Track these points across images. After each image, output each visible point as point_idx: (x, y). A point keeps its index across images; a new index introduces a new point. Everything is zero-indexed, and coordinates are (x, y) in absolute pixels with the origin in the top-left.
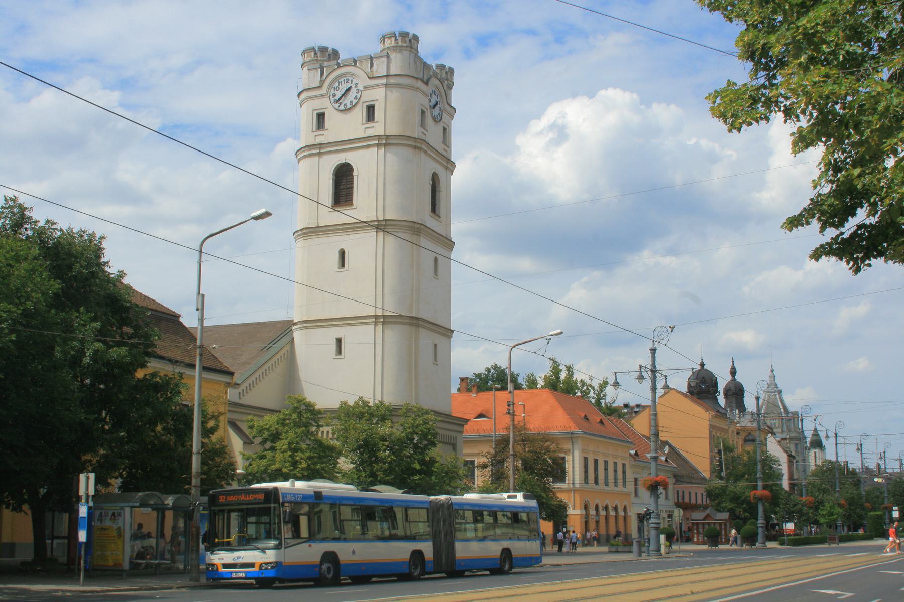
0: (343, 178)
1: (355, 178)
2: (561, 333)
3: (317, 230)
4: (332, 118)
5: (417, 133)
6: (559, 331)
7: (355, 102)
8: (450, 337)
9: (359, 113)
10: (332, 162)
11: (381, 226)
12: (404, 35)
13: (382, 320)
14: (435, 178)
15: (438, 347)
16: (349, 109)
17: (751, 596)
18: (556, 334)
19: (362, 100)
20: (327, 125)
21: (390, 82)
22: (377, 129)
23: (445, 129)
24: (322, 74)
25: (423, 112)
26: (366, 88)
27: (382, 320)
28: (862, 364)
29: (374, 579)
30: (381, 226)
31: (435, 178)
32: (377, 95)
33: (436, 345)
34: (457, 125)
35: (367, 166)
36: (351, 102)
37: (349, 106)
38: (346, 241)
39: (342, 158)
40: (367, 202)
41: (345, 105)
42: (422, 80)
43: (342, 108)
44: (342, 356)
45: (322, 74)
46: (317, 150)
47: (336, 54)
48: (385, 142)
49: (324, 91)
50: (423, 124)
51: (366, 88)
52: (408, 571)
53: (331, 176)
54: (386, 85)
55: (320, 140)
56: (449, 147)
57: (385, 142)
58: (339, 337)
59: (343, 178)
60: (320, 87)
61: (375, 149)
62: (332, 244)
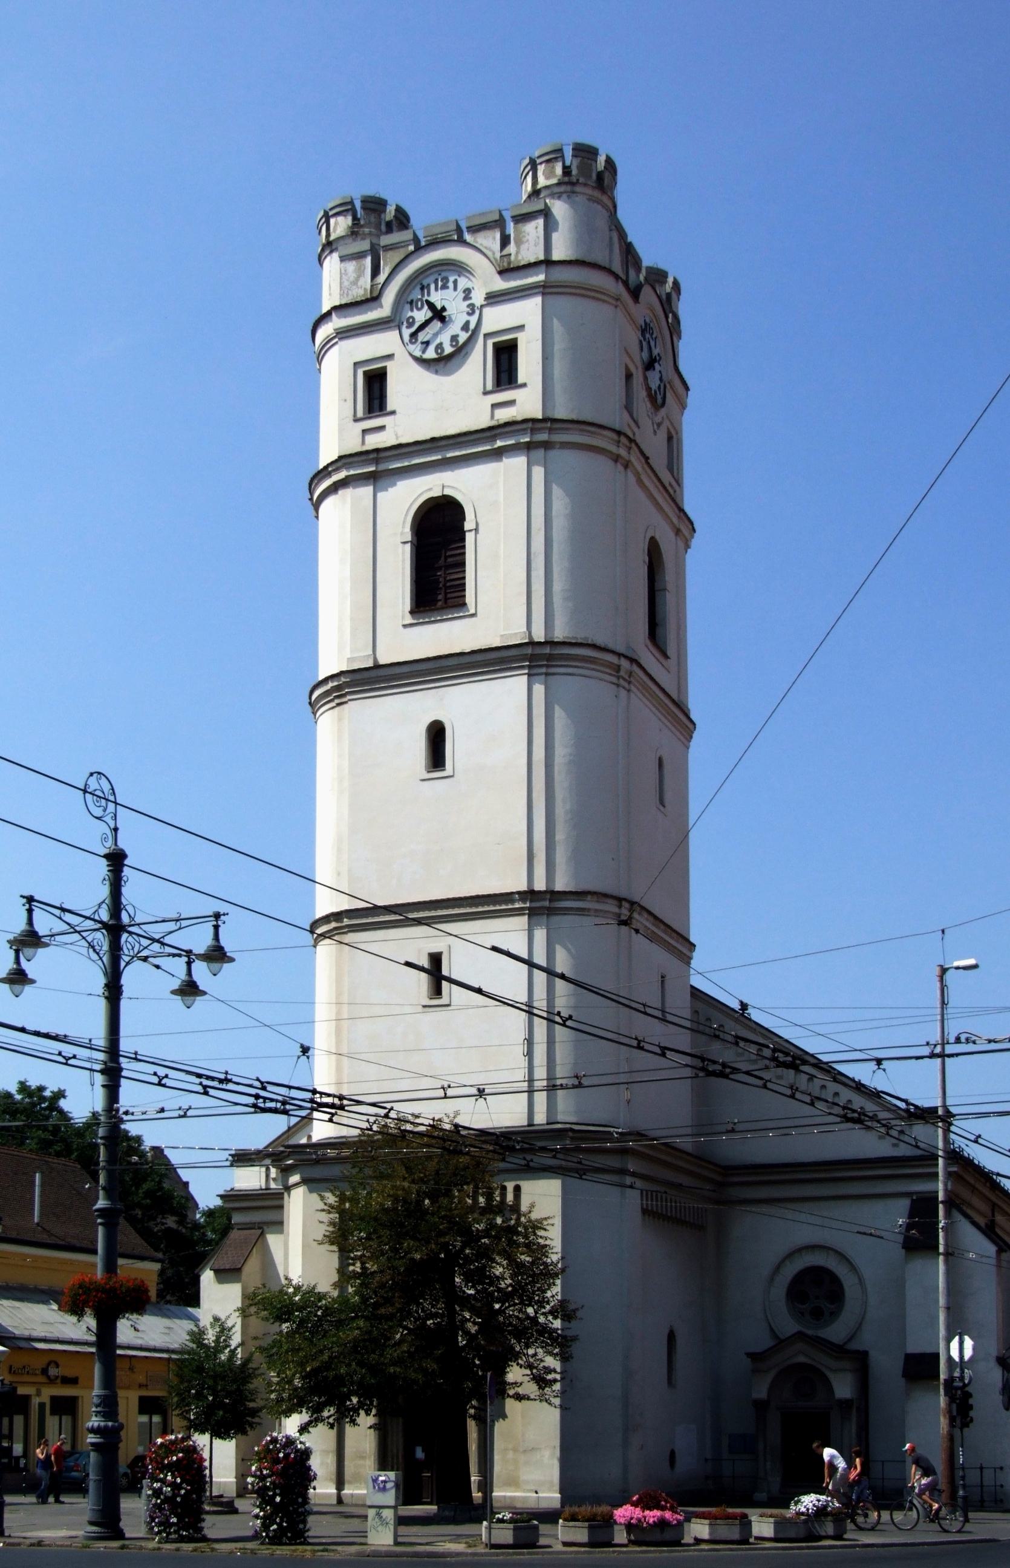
0: (439, 536)
1: (469, 538)
2: (975, 966)
3: (373, 673)
4: (406, 382)
5: (616, 418)
6: (971, 962)
7: (463, 337)
9: (478, 365)
10: (407, 495)
11: (533, 657)
12: (586, 152)
13: (538, 905)
14: (654, 551)
16: (451, 356)
18: (965, 968)
19: (486, 328)
20: (393, 401)
21: (553, 281)
22: (527, 402)
23: (670, 438)
24: (376, 271)
25: (629, 376)
26: (494, 298)
27: (538, 905)
30: (533, 657)
31: (654, 551)
32: (526, 316)
35: (499, 500)
36: (454, 338)
37: (448, 349)
38: (456, 703)
40: (502, 596)
41: (440, 346)
42: (626, 283)
43: (431, 354)
45: (376, 271)
46: (374, 467)
47: (402, 220)
48: (536, 437)
49: (385, 309)
50: (628, 407)
51: (494, 298)
55: (374, 441)
56: (679, 482)
57: (536, 437)
59: (439, 536)
62: (408, 712)
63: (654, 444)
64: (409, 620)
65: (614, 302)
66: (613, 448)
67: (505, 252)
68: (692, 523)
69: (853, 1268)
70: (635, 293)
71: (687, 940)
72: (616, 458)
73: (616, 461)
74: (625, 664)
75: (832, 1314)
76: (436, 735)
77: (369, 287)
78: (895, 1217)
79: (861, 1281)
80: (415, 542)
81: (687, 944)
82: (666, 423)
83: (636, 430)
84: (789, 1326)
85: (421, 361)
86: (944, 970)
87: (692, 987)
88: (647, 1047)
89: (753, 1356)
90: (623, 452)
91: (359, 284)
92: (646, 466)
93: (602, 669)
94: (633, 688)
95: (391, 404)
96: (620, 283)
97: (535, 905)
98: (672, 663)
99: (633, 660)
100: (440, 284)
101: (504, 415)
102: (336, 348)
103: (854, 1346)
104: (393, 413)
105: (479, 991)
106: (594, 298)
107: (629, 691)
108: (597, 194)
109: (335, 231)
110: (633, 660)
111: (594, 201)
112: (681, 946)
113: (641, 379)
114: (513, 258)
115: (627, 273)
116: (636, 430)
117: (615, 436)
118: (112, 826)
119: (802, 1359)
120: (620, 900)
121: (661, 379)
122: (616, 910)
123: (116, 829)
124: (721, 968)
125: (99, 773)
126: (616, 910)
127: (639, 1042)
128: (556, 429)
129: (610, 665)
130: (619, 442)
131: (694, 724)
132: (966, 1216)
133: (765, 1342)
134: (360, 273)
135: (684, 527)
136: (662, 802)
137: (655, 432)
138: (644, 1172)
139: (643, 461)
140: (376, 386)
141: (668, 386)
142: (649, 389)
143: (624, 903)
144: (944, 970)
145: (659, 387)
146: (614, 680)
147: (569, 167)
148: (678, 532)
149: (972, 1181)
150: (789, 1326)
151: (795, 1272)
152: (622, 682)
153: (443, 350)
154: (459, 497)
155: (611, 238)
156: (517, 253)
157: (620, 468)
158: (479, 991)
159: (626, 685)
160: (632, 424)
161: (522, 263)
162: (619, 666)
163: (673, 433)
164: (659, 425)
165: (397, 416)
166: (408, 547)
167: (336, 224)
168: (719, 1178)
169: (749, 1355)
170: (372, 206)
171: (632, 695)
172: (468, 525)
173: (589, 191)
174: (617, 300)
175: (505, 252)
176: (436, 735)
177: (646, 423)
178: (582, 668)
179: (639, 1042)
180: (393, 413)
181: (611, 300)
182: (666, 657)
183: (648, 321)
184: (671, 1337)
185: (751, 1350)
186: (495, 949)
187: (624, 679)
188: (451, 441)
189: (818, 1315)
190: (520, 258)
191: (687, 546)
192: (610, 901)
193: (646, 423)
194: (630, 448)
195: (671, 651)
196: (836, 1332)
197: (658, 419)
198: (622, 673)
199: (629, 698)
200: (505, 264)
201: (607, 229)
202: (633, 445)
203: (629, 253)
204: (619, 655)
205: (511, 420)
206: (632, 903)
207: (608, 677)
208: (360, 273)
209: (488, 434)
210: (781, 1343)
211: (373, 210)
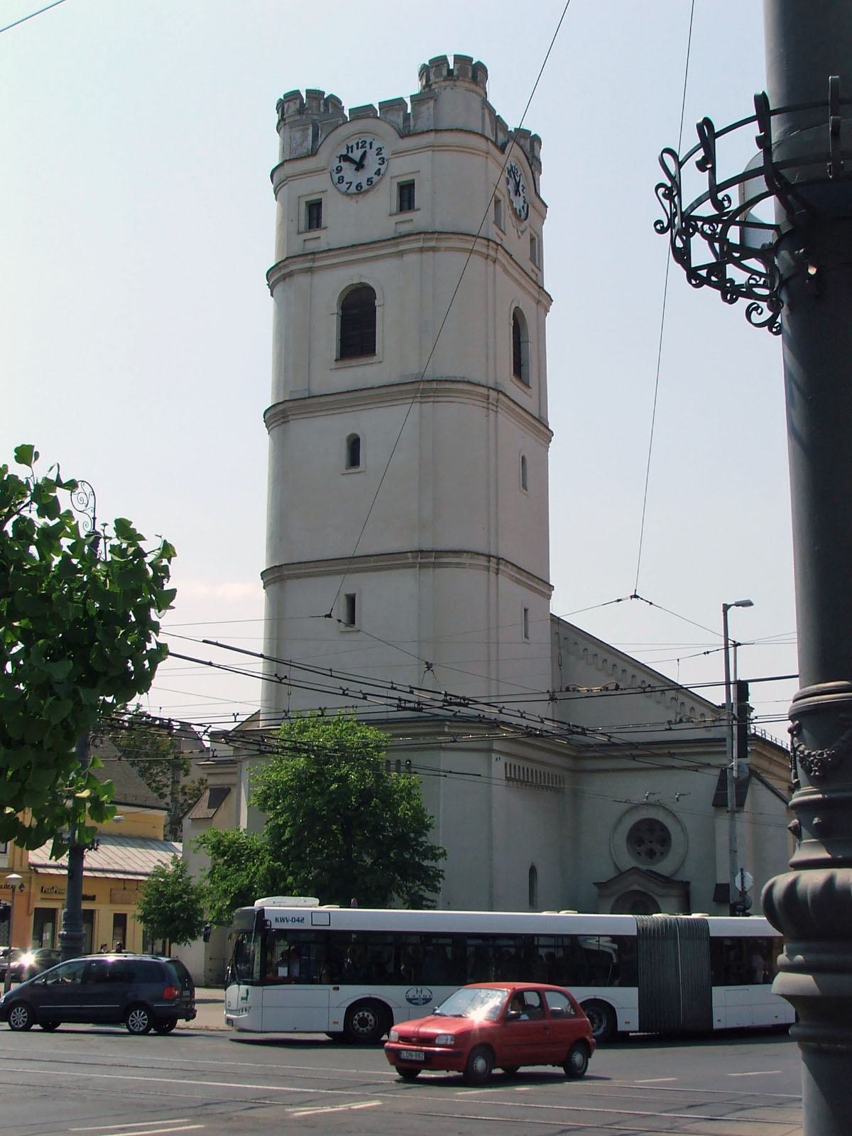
3: (310, 401)
8: (549, 597)
9: (386, 196)
10: (330, 286)
15: (529, 612)
17: (166, 1133)
23: (532, 240)
26: (397, 153)
28: (840, 856)
29: (424, 1074)
33: (526, 610)
34: (549, 231)
39: (361, 373)
42: (495, 144)
44: (357, 625)
50: (497, 222)
52: (724, 686)
53: (335, 308)
54: (433, 151)
55: (311, 246)
56: (540, 269)
58: (350, 592)
60: (313, 153)
61: (418, 404)
62: (336, 428)
63: (519, 248)
64: (334, 365)
65: (485, 155)
66: (484, 250)
67: (364, 150)
68: (550, 296)
69: (679, 821)
70: (502, 149)
71: (548, 584)
72: (487, 257)
73: (487, 258)
74: (493, 394)
75: (662, 854)
76: (354, 445)
77: (310, 148)
78: (706, 782)
79: (684, 830)
80: (340, 314)
81: (547, 586)
82: (529, 230)
83: (503, 237)
84: (627, 861)
85: (347, 194)
86: (726, 608)
87: (551, 614)
88: (350, 693)
89: (599, 885)
90: (492, 253)
91: (304, 145)
92: (511, 261)
93: (478, 398)
94: (499, 410)
95: (324, 222)
96: (490, 144)
97: (423, 561)
98: (534, 391)
99: (499, 391)
100: (360, 145)
101: (405, 228)
102: (286, 186)
103: (679, 877)
104: (326, 228)
105: (210, 664)
106: (470, 153)
107: (496, 412)
108: (473, 87)
109: (287, 112)
110: (499, 391)
111: (470, 91)
112: (544, 589)
113: (508, 203)
114: (411, 128)
115: (496, 136)
116: (503, 237)
117: (485, 242)
118: (92, 516)
119: (636, 887)
120: (489, 556)
121: (524, 202)
122: (487, 564)
123: (94, 518)
124: (560, 606)
125: (83, 481)
126: (487, 564)
127: (344, 691)
128: (440, 239)
129: (481, 395)
130: (488, 245)
131: (552, 432)
132: (763, 781)
133: (608, 873)
134: (305, 138)
135: (544, 301)
136: (525, 486)
137: (519, 237)
138: (506, 750)
139: (508, 257)
140: (315, 212)
141: (530, 205)
142: (514, 210)
143: (492, 558)
144: (726, 608)
145: (523, 207)
146: (485, 405)
147: (452, 70)
148: (538, 302)
149: (769, 755)
150: (627, 861)
151: (633, 822)
152: (491, 406)
153: (361, 187)
154: (372, 284)
155: (483, 115)
156: (415, 125)
157: (490, 263)
158: (210, 664)
159: (494, 408)
160: (500, 233)
161: (419, 131)
162: (488, 396)
163: (535, 236)
164: (522, 232)
165: (328, 229)
166: (335, 317)
167: (288, 107)
168: (574, 754)
169: (595, 884)
170: (312, 95)
171: (500, 416)
172: (377, 303)
173: (467, 85)
174: (487, 153)
175: (364, 150)
176: (354, 445)
177: (511, 231)
178: (459, 397)
179: (344, 691)
180: (326, 228)
181: (482, 154)
182: (527, 386)
183: (513, 165)
184: (533, 871)
185: (595, 882)
186: (204, 641)
187: (493, 404)
188: (366, 247)
189: (651, 854)
190: (417, 127)
191: (547, 311)
192: (482, 557)
193: (511, 231)
194: (497, 250)
195: (533, 381)
196: (665, 867)
197: (522, 228)
198: (490, 400)
199: (496, 417)
200: (407, 132)
201: (480, 109)
202: (499, 247)
203: (498, 122)
204: (489, 388)
205: (410, 232)
206: (499, 559)
207: (481, 404)
208: (305, 138)
209: (392, 242)
210: (621, 875)
211: (315, 98)
